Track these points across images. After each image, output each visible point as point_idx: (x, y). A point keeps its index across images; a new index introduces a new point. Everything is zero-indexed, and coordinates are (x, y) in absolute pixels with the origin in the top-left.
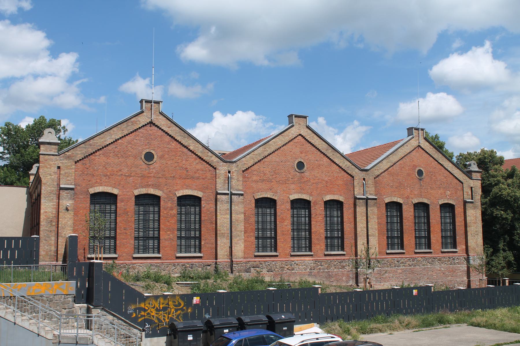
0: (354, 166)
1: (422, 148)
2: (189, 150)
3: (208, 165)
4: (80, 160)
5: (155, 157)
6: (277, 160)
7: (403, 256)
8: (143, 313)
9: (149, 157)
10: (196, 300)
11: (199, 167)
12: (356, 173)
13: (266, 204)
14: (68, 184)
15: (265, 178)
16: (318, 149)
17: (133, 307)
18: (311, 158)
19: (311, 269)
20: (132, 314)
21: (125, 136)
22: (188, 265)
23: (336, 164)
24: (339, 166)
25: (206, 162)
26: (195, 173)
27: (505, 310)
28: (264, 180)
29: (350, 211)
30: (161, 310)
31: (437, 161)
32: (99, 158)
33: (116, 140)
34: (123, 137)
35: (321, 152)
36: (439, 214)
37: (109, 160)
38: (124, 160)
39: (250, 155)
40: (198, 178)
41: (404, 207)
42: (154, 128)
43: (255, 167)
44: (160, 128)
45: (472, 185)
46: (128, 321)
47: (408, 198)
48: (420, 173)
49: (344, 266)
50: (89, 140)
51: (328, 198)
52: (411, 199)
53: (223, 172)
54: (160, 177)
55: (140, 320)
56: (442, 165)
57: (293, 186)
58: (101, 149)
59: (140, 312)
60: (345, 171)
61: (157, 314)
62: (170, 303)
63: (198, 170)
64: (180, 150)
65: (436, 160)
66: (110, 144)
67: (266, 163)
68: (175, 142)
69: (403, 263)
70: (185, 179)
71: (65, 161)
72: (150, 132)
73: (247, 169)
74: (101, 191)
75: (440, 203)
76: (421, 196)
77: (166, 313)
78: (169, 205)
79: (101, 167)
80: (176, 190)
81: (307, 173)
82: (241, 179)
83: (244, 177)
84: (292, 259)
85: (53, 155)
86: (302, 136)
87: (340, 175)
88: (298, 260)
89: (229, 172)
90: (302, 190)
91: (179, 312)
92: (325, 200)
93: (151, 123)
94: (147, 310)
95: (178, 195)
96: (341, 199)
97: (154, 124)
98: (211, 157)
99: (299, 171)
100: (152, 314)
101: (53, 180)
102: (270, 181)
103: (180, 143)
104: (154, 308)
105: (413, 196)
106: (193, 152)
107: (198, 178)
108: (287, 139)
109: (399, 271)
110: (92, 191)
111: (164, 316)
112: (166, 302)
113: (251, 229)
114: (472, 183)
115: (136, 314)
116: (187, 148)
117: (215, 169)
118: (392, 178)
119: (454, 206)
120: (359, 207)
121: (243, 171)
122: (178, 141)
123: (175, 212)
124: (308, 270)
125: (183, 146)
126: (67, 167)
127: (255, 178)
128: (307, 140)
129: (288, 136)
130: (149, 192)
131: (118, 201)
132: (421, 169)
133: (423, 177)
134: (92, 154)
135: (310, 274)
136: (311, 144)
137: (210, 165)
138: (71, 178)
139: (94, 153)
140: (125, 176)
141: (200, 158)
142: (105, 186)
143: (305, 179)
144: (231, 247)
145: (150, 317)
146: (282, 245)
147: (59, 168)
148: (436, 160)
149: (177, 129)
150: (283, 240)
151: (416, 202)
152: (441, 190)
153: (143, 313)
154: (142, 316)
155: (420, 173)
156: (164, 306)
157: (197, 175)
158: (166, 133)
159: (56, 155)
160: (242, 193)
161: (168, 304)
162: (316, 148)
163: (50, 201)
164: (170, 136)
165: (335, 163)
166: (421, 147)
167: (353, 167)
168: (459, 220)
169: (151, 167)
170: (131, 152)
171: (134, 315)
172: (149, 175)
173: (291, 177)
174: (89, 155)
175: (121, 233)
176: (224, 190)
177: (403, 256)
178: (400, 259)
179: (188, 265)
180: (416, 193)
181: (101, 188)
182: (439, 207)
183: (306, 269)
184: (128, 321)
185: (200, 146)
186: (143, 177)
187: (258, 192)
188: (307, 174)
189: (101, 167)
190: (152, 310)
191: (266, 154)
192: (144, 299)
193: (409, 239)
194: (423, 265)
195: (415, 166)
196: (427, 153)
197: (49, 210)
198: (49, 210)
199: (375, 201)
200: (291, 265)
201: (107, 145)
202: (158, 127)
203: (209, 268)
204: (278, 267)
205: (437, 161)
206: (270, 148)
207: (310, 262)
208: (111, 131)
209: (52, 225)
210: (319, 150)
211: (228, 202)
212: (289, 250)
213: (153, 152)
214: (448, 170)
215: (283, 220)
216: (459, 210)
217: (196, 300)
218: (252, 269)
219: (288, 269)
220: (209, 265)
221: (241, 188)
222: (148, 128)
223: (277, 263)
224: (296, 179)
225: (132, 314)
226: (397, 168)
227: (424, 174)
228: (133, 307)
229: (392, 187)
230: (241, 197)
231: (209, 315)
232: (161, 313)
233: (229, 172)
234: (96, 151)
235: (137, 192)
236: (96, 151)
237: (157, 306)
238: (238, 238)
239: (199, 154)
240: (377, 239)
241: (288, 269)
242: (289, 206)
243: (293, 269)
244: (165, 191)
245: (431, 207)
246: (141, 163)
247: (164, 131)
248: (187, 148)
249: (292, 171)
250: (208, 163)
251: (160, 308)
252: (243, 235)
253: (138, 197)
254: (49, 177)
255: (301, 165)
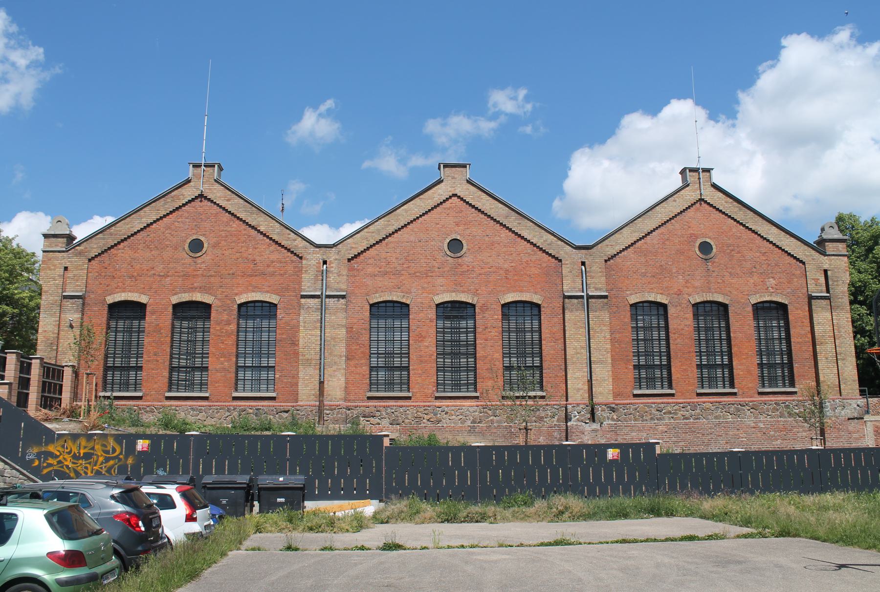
0: (562, 241)
1: (709, 204)
2: (259, 231)
3: (289, 254)
4: (96, 256)
5: (206, 245)
6: (412, 238)
7: (671, 401)
8: (51, 461)
9: (196, 246)
10: (142, 445)
11: (274, 257)
12: (566, 253)
13: (390, 311)
14: (77, 291)
15: (388, 270)
16: (489, 216)
17: (35, 450)
18: (473, 232)
19: (474, 422)
20: (32, 461)
21: (161, 218)
22: (251, 411)
23: (526, 240)
24: (532, 243)
25: (286, 248)
26: (268, 266)
27: (676, 452)
28: (386, 273)
29: (556, 320)
30: (82, 458)
31: (744, 226)
32: (123, 253)
33: (148, 225)
34: (158, 220)
35: (495, 220)
36: (753, 323)
37: (137, 255)
38: (158, 252)
39: (362, 233)
40: (273, 274)
41: (671, 311)
42: (205, 202)
43: (372, 252)
44: (215, 203)
45: (826, 267)
46: (25, 472)
47: (679, 293)
48: (705, 248)
49: (542, 417)
50: (109, 228)
51: (510, 298)
52: (686, 296)
53: (313, 262)
54: (211, 276)
55: (45, 471)
56: (753, 231)
57: (440, 281)
58: (125, 239)
59: (46, 459)
60: (544, 251)
61: (73, 463)
62: (96, 447)
63: (273, 262)
64: (244, 232)
65: (741, 224)
66: (139, 231)
67: (392, 245)
68: (238, 222)
69: (670, 413)
70: (251, 276)
71: (75, 259)
72: (200, 210)
73: (356, 256)
74: (123, 299)
75: (753, 301)
76: (709, 290)
77: (90, 463)
78: (225, 317)
79: (125, 266)
80: (236, 294)
81: (468, 258)
82: (345, 272)
83: (351, 269)
84: (438, 403)
85: (59, 252)
86: (459, 197)
87: (534, 258)
88: (448, 406)
89: (325, 262)
90: (458, 286)
91: (112, 462)
92: (503, 302)
93: (201, 196)
94: (58, 456)
95: (239, 302)
96: (536, 299)
97: (206, 198)
98: (295, 240)
99: (452, 255)
100: (66, 463)
101: (57, 286)
102: (398, 274)
103: (244, 222)
104: (69, 453)
105: (690, 290)
106: (265, 235)
107: (273, 274)
108: (431, 204)
109: (660, 428)
110: (110, 300)
111: (86, 468)
112: (91, 445)
113: (362, 353)
114: (826, 262)
115: (40, 461)
116: (256, 229)
117: (301, 258)
118: (643, 260)
119: (786, 305)
120: (572, 311)
121: (349, 260)
122: (241, 220)
123: (233, 327)
124: (469, 423)
125: (250, 226)
126: (77, 268)
127: (370, 270)
128: (467, 203)
129: (432, 198)
130: (194, 299)
131: (147, 313)
132: (708, 240)
133: (712, 255)
134: (112, 247)
135: (472, 431)
136: (476, 209)
137: (292, 252)
138: (82, 283)
139: (116, 245)
140: (160, 276)
141: (277, 243)
142: (130, 291)
143: (465, 268)
144: (321, 383)
145: (62, 467)
146: (419, 380)
147: (66, 269)
148: (741, 224)
149: (241, 201)
150: (420, 372)
151: (698, 301)
152: (755, 278)
153: (51, 461)
154: (50, 465)
155: (705, 248)
156: (86, 451)
157: (271, 269)
158: (224, 209)
159: (63, 252)
160: (344, 293)
161: (93, 448)
162: (486, 214)
163: (52, 315)
164: (230, 212)
165: (523, 238)
166: (706, 202)
167: (560, 242)
168: (799, 332)
169: (199, 261)
170: (170, 241)
171: (37, 463)
172: (195, 273)
173: (437, 265)
174: (109, 249)
175: (149, 361)
176: (315, 290)
177: (671, 401)
178: (663, 405)
179: (251, 411)
180: (697, 284)
181: (123, 294)
182: (750, 309)
183: (463, 422)
184: (25, 472)
185: (277, 224)
186: (186, 276)
187: (376, 292)
188: (468, 259)
189: (125, 266)
190: (66, 456)
191: (391, 229)
192: (51, 436)
193: (685, 369)
194: (716, 417)
195: (695, 236)
196: (721, 211)
197: (50, 328)
198: (50, 328)
199: (605, 300)
200: (435, 415)
201: (136, 233)
202: (212, 201)
203: (285, 415)
204: (409, 417)
205: (744, 226)
206: (397, 220)
207: (471, 409)
208: (142, 213)
209: (52, 350)
210: (492, 218)
211: (317, 309)
212: (431, 389)
213: (202, 238)
214: (768, 241)
215: (421, 338)
216: (797, 314)
217: (142, 445)
218: (362, 419)
219: (428, 420)
220: (287, 412)
221: (344, 287)
222: (197, 203)
223: (408, 410)
224: (446, 269)
225: (32, 461)
226: (655, 242)
227: (714, 250)
228: (35, 450)
229: (644, 275)
230: (342, 301)
231: (165, 470)
232: (80, 461)
233: (325, 262)
234: (119, 243)
235: (175, 300)
236: (119, 243)
237: (75, 450)
238: (335, 368)
239: (275, 237)
240: (609, 368)
241: (428, 420)
242: (432, 314)
243: (439, 421)
244: (219, 296)
245: (731, 310)
246: (184, 254)
247: (221, 207)
248: (256, 229)
249: (440, 257)
250: (289, 250)
251: (80, 453)
252: (343, 362)
253: (177, 307)
254: (52, 283)
255: (455, 245)
